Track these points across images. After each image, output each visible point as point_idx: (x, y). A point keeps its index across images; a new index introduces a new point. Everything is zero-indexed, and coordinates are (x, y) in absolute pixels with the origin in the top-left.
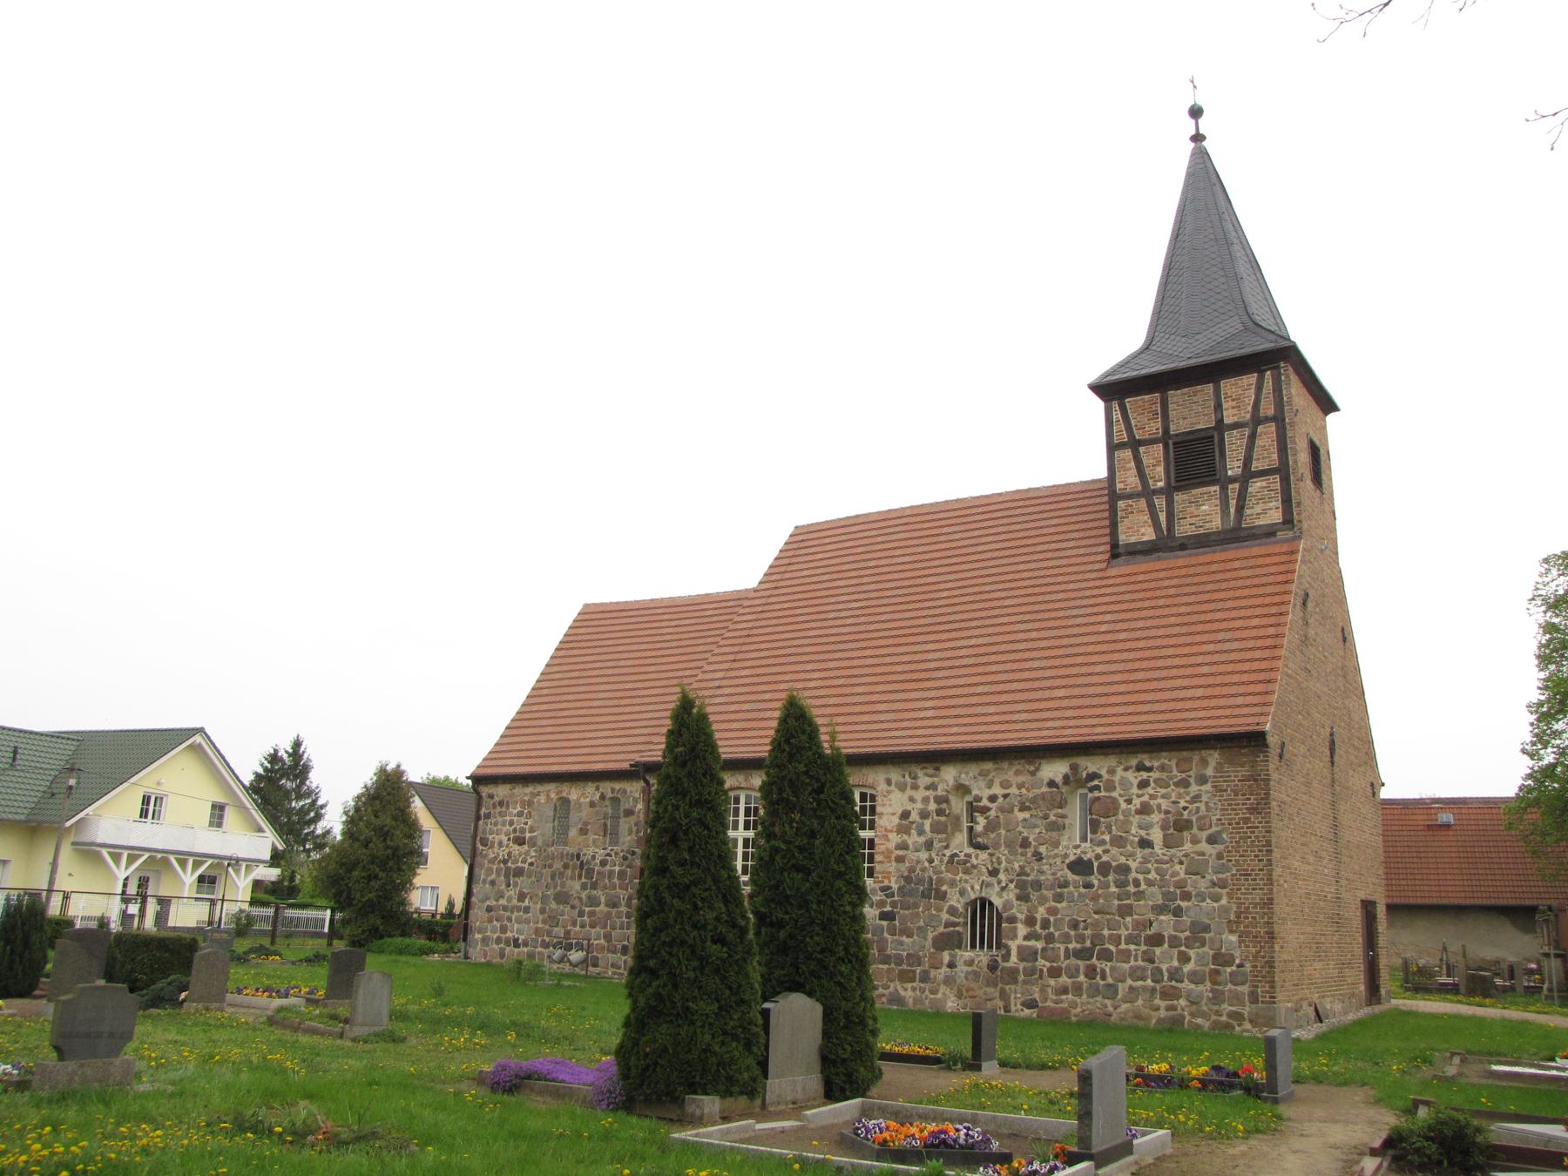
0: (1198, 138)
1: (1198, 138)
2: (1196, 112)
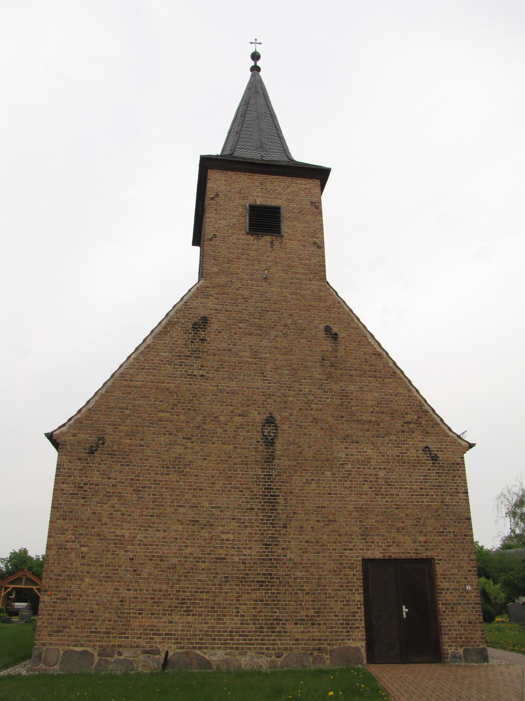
0: (255, 69)
1: (255, 69)
2: (255, 56)
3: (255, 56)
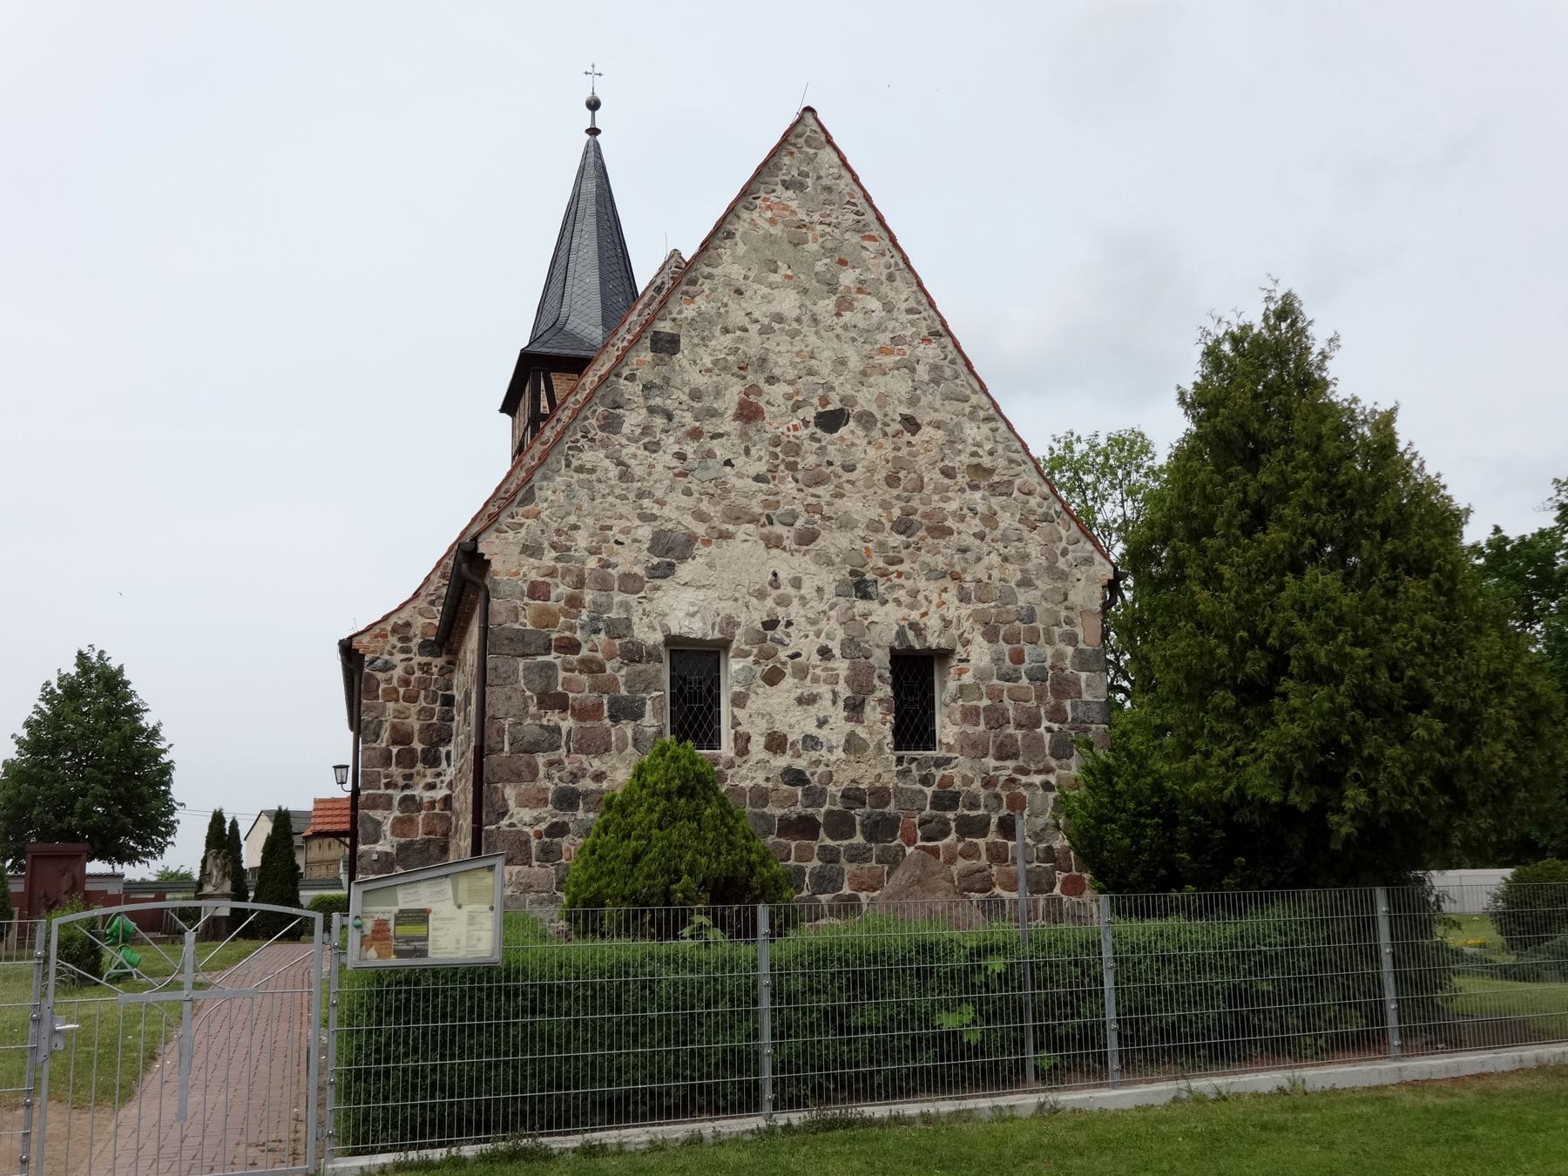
1: (594, 131)
2: (594, 105)
3: (594, 105)
